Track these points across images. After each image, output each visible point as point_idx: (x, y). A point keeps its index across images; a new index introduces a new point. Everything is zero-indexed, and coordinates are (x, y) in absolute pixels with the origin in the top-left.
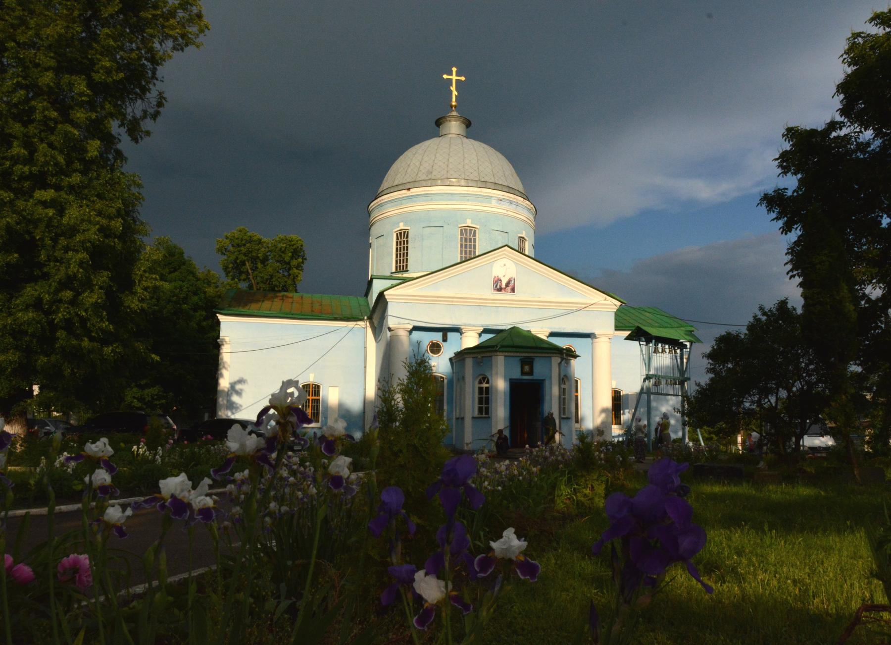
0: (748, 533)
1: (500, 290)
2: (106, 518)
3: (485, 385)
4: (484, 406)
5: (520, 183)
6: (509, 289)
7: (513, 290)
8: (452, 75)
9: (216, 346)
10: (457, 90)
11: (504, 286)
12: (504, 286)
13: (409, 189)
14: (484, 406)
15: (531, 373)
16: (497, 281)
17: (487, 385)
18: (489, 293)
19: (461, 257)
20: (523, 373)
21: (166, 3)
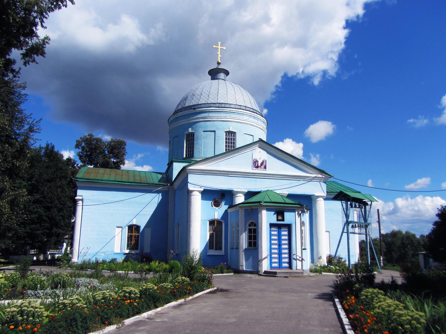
0: (439, 307)
1: (257, 167)
2: (301, 145)
3: (253, 227)
4: (253, 241)
5: (252, 100)
6: (263, 167)
7: (265, 167)
8: (218, 46)
9: (75, 202)
10: (220, 54)
11: (259, 165)
12: (259, 165)
13: (195, 109)
14: (253, 241)
15: (283, 220)
16: (255, 162)
17: (255, 227)
18: (250, 169)
19: (226, 149)
20: (278, 220)
21: (21, 2)
